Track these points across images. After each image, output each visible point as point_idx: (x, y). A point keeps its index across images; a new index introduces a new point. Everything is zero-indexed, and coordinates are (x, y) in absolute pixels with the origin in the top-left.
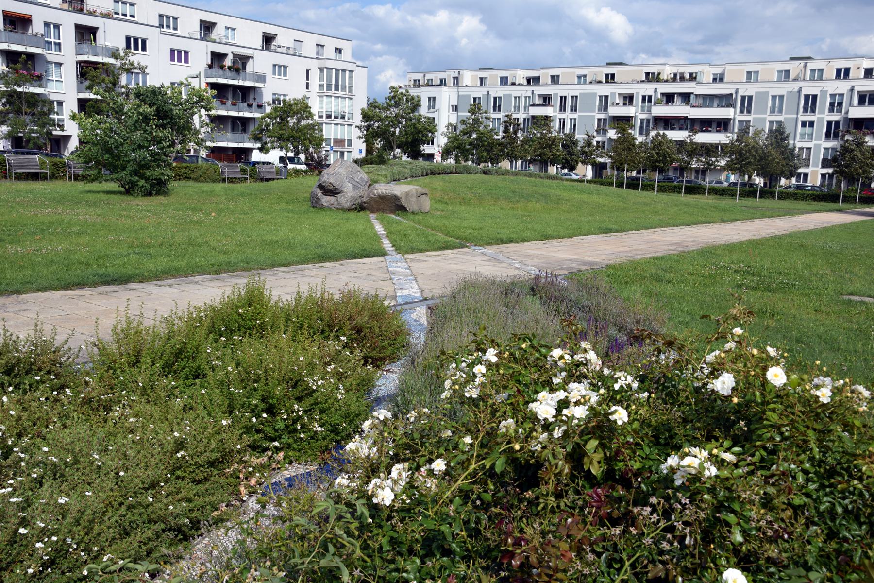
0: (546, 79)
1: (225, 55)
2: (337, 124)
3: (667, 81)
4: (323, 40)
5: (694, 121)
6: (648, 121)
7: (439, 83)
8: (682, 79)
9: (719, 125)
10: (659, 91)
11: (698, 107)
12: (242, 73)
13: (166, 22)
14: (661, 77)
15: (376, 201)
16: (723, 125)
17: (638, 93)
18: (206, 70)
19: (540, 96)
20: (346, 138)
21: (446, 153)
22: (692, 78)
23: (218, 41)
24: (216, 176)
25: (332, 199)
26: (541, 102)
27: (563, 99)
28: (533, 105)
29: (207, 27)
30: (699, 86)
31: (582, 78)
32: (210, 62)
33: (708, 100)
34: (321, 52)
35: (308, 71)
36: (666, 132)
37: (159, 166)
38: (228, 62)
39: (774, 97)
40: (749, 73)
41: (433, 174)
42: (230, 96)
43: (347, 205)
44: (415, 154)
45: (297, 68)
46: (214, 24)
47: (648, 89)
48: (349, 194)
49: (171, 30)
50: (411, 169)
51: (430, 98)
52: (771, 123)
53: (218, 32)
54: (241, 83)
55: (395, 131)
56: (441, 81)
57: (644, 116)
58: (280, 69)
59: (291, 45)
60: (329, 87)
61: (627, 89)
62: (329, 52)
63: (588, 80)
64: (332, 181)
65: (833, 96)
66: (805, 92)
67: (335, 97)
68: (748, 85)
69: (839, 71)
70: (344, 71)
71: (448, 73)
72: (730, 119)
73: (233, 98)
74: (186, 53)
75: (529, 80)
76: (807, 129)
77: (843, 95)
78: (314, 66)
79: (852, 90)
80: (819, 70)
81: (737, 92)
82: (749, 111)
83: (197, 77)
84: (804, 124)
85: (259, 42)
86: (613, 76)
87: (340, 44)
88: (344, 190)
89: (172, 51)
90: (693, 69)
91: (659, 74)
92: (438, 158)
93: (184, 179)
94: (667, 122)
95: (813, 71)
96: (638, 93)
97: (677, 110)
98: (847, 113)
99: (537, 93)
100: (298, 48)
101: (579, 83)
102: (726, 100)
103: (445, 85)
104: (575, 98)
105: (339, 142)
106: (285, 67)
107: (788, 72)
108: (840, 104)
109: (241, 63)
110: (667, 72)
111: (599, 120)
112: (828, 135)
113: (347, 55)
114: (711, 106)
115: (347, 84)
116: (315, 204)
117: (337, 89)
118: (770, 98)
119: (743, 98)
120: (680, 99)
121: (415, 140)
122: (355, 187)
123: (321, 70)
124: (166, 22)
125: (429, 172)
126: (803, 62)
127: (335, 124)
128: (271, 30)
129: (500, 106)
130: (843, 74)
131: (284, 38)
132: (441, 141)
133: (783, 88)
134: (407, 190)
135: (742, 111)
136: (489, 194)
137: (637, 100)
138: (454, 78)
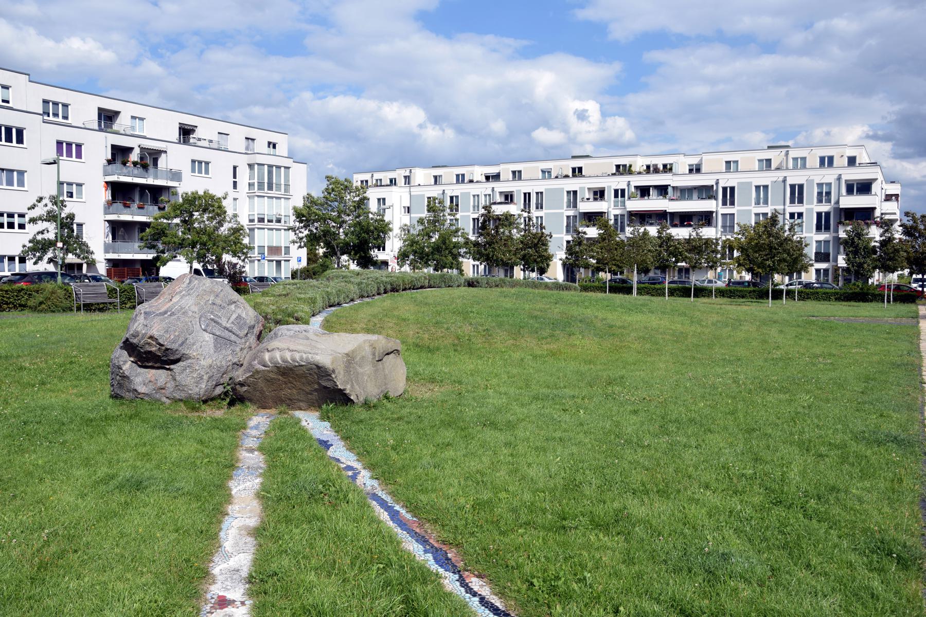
0: (506, 174)
1: (130, 149)
2: (272, 229)
3: (640, 173)
4: (253, 133)
5: (673, 214)
6: (622, 216)
7: (389, 183)
8: (656, 171)
10: (633, 184)
11: (677, 200)
12: (151, 169)
13: (52, 110)
14: (633, 169)
15: (269, 381)
16: (706, 218)
17: (609, 187)
19: (501, 193)
20: (283, 246)
21: (402, 257)
22: (667, 169)
23: (122, 132)
24: (66, 303)
25: (160, 376)
26: (503, 200)
27: (527, 196)
28: (495, 203)
29: (107, 117)
30: (675, 178)
32: (110, 157)
33: (686, 192)
34: (251, 147)
35: (235, 168)
38: (134, 156)
39: (758, 187)
40: (728, 163)
41: (394, 290)
42: (137, 198)
43: (200, 389)
44: (366, 261)
45: (221, 164)
47: (621, 182)
49: (60, 119)
50: (359, 284)
51: (379, 200)
52: (757, 215)
54: (150, 181)
56: (391, 181)
57: (618, 212)
58: (200, 166)
59: (215, 137)
60: (261, 185)
61: (597, 184)
62: (261, 145)
63: (553, 175)
64: (155, 332)
65: (820, 185)
66: (790, 181)
67: (269, 197)
68: (728, 176)
69: (822, 160)
70: (279, 167)
71: (398, 171)
72: (712, 212)
73: (141, 199)
74: (79, 146)
77: (830, 184)
78: (242, 163)
80: (801, 158)
81: (717, 183)
82: (732, 203)
83: (54, 163)
84: (792, 215)
85: (175, 134)
86: (580, 169)
87: (274, 137)
88: (192, 353)
90: (667, 160)
91: (630, 166)
92: (393, 265)
93: (15, 307)
94: (643, 217)
95: (795, 159)
96: (609, 187)
98: (838, 202)
99: (497, 190)
100: (222, 142)
101: (544, 178)
102: (706, 192)
103: (395, 184)
105: (274, 250)
106: (207, 163)
107: (769, 161)
108: (828, 194)
109: (150, 158)
110: (639, 164)
111: (568, 217)
112: (819, 228)
113: (282, 149)
114: (690, 198)
115: (283, 182)
117: (270, 187)
118: (754, 188)
119: (725, 189)
120: (656, 192)
121: (364, 242)
122: (221, 342)
123: (251, 166)
124: (52, 110)
125: (389, 287)
126: (784, 150)
127: (269, 229)
128: (189, 120)
130: (827, 162)
131: (205, 129)
132: (393, 245)
134: (348, 348)
135: (724, 203)
136: (500, 325)
137: (610, 195)
138: (405, 177)
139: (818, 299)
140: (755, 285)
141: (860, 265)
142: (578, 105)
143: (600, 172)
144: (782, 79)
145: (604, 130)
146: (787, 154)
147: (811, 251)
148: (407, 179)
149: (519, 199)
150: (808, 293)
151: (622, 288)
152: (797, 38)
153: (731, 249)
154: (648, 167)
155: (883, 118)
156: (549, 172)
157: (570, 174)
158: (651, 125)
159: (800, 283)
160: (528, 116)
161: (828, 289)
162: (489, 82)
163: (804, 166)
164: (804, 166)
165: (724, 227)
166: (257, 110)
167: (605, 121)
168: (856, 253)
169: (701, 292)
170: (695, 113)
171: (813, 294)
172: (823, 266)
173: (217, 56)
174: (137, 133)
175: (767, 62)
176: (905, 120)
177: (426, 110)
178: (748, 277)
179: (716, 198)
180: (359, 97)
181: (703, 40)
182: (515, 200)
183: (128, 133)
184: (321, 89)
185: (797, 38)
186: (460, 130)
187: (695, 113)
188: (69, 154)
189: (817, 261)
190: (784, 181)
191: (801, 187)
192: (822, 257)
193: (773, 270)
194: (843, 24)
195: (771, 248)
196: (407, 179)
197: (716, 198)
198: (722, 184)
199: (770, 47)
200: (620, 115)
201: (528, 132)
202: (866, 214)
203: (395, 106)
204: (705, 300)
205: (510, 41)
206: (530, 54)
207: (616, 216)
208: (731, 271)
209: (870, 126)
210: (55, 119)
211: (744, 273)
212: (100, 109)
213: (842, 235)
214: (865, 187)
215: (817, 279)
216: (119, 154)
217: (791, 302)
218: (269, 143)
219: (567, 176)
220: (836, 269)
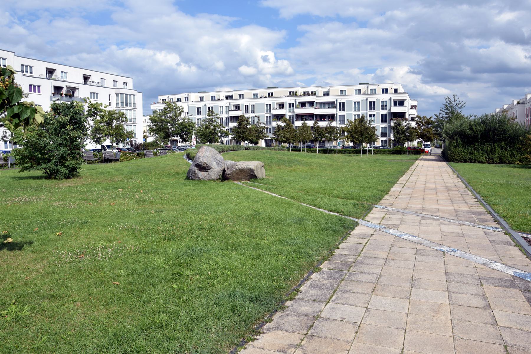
1: (62, 88)
3: (300, 96)
5: (316, 115)
6: (293, 116)
7: (177, 100)
8: (308, 95)
9: (329, 118)
10: (298, 101)
14: (297, 93)
15: (237, 173)
16: (332, 117)
17: (286, 102)
18: (51, 96)
19: (234, 105)
22: (313, 94)
25: (205, 173)
26: (235, 109)
27: (247, 107)
28: (231, 110)
29: (50, 72)
30: (317, 98)
31: (256, 95)
32: (53, 92)
33: (322, 105)
35: (110, 95)
36: (306, 122)
37: (74, 158)
38: (64, 91)
39: (355, 103)
40: (341, 91)
43: (215, 176)
46: (54, 70)
47: (292, 100)
48: (216, 170)
49: (29, 74)
52: (355, 115)
53: (57, 74)
55: (169, 129)
56: (178, 99)
57: (291, 114)
59: (100, 81)
61: (281, 101)
62: (120, 85)
63: (259, 96)
65: (382, 102)
66: (369, 100)
68: (342, 97)
69: (383, 90)
70: (130, 95)
71: (182, 95)
72: (334, 114)
74: (39, 87)
75: (227, 98)
76: (373, 118)
78: (113, 92)
79: (390, 99)
81: (337, 101)
82: (344, 110)
84: (370, 116)
85: (81, 80)
86: (272, 94)
89: (30, 86)
94: (300, 117)
95: (371, 90)
97: (308, 110)
98: (390, 110)
101: (254, 98)
102: (332, 105)
103: (180, 101)
104: (253, 106)
106: (97, 94)
107: (360, 90)
108: (386, 106)
110: (300, 91)
112: (382, 121)
114: (324, 108)
115: (132, 102)
116: (190, 176)
117: (127, 105)
119: (340, 103)
123: (117, 95)
126: (366, 86)
128: (87, 73)
129: (200, 111)
130: (385, 91)
131: (95, 77)
133: (359, 98)
134: (256, 165)
135: (340, 110)
137: (286, 106)
138: (185, 98)
139: (381, 153)
140: (355, 148)
141: (400, 138)
142: (264, 54)
143: (281, 95)
144: (369, 41)
145: (277, 67)
146: (368, 87)
147: (378, 133)
148: (187, 98)
149: (243, 108)
150: (377, 151)
151: (295, 149)
152: (378, 20)
153: (344, 131)
154: (304, 93)
155: (418, 62)
156: (257, 95)
157: (267, 96)
158: (301, 64)
159: (374, 147)
160: (235, 60)
161: (386, 149)
162: (216, 41)
163: (375, 93)
164: (375, 93)
165: (340, 121)
166: (84, 55)
167: (277, 62)
168: (398, 133)
169: (332, 151)
170: (325, 58)
171: (379, 151)
172: (384, 139)
173: (60, 24)
174: (64, 80)
175: (362, 32)
176: (428, 64)
177: (180, 56)
178: (351, 144)
179: (336, 108)
180: (143, 48)
181: (329, 19)
182: (241, 108)
183: (60, 79)
184: (122, 44)
185: (378, 20)
186: (199, 67)
187: (325, 58)
188: (35, 91)
189: (381, 136)
190: (367, 100)
191: (374, 102)
192: (384, 134)
193: (362, 141)
194: (399, 14)
195: (361, 132)
196: (187, 98)
197: (336, 108)
198: (339, 101)
199: (363, 24)
200: (285, 59)
201: (236, 68)
202: (402, 115)
203: (163, 53)
204: (334, 155)
205: (227, 18)
206: (237, 25)
207: (290, 116)
208: (343, 142)
209: (410, 67)
210: (27, 74)
211: (350, 143)
212: (47, 68)
213: (392, 124)
214: (401, 103)
215: (382, 145)
216: (57, 89)
217: (370, 155)
218: (124, 83)
219: (266, 97)
220: (390, 140)
